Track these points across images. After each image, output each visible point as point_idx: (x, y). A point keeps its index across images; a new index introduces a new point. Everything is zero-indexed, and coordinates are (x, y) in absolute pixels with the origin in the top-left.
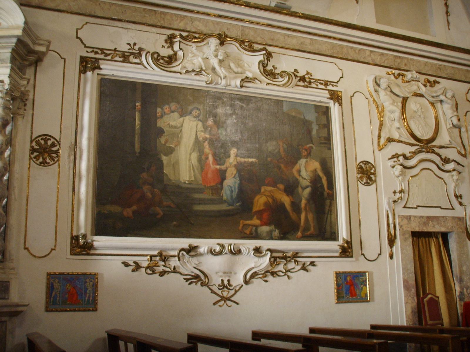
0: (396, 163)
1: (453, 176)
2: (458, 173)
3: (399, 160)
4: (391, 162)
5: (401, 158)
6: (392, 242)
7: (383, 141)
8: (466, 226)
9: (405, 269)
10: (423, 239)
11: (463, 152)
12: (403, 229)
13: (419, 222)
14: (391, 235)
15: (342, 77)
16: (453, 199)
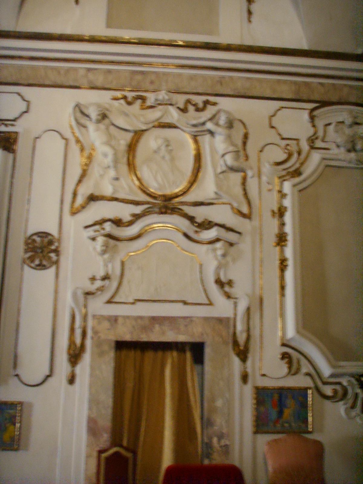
0: (97, 233)
1: (215, 250)
2: (227, 244)
3: (103, 229)
4: (91, 232)
5: (108, 227)
6: (75, 356)
7: (80, 200)
8: (235, 334)
9: (93, 401)
10: (135, 353)
11: (245, 210)
12: (99, 337)
13: (134, 327)
14: (75, 345)
15: (26, 112)
16: (214, 289)
